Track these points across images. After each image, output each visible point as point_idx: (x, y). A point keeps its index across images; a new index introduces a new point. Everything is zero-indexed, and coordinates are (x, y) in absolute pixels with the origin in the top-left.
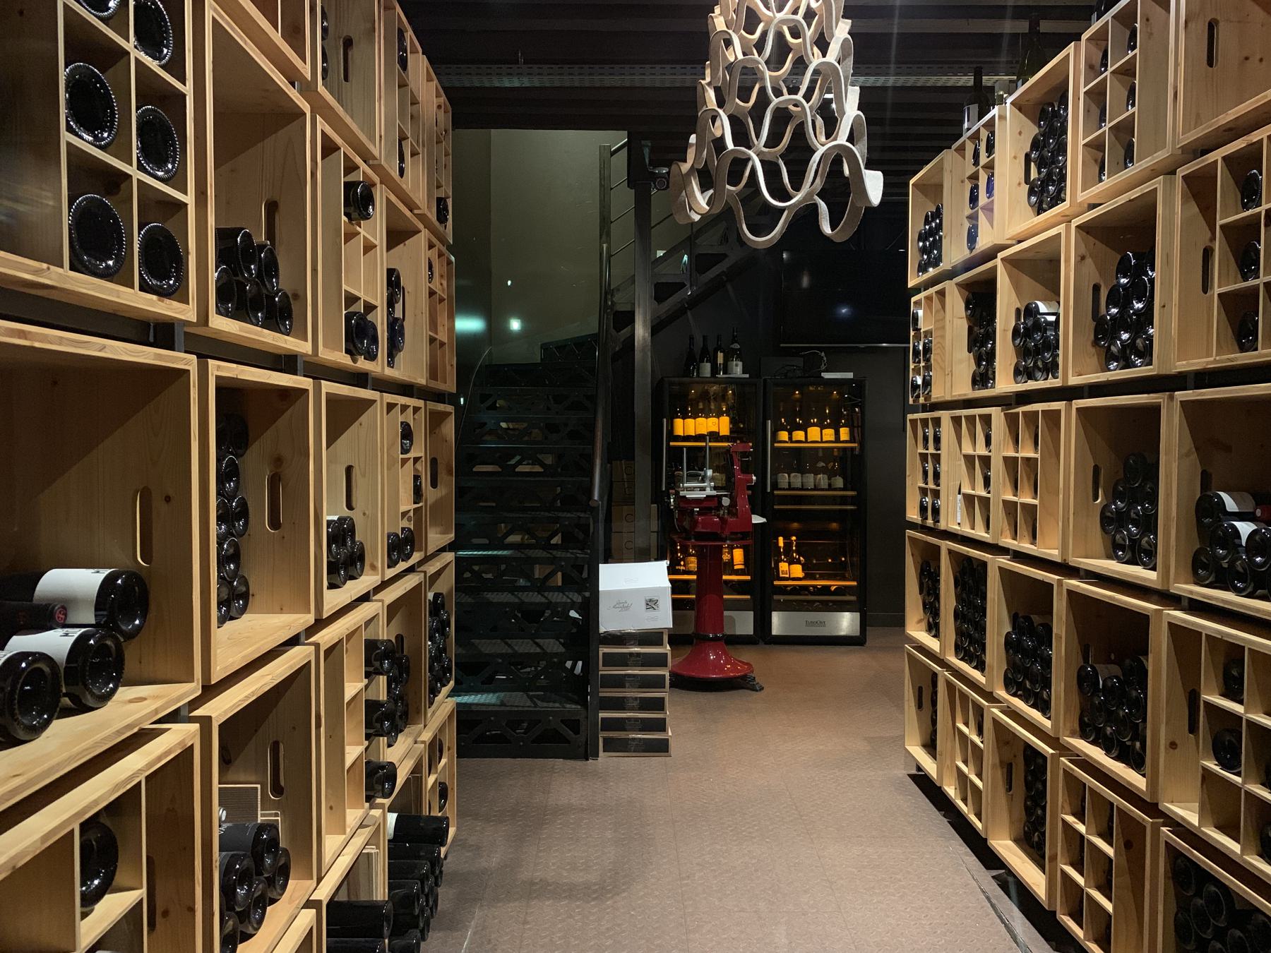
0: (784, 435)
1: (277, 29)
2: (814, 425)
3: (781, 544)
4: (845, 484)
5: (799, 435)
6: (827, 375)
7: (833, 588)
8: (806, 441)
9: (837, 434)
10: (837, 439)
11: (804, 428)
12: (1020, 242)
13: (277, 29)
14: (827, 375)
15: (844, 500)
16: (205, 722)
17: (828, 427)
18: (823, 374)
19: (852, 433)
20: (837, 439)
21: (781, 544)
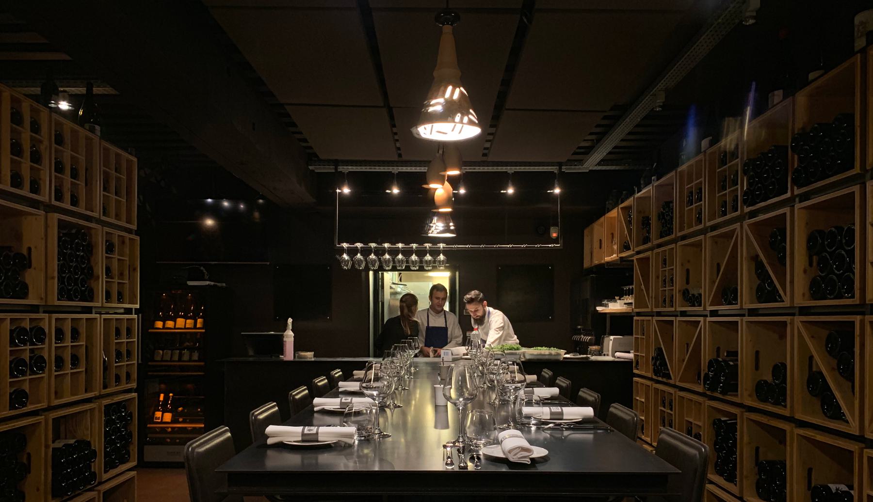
0: (159, 324)
1: (599, 164)
2: (181, 317)
3: (162, 398)
4: (199, 357)
5: (170, 324)
6: (190, 283)
7: (170, 430)
8: (175, 328)
9: (196, 323)
10: (195, 327)
11: (174, 319)
12: (86, 170)
13: (599, 164)
14: (190, 283)
15: (199, 368)
16: (99, 491)
17: (190, 318)
18: (477, 292)
19: (204, 323)
20: (195, 327)
21: (162, 398)
